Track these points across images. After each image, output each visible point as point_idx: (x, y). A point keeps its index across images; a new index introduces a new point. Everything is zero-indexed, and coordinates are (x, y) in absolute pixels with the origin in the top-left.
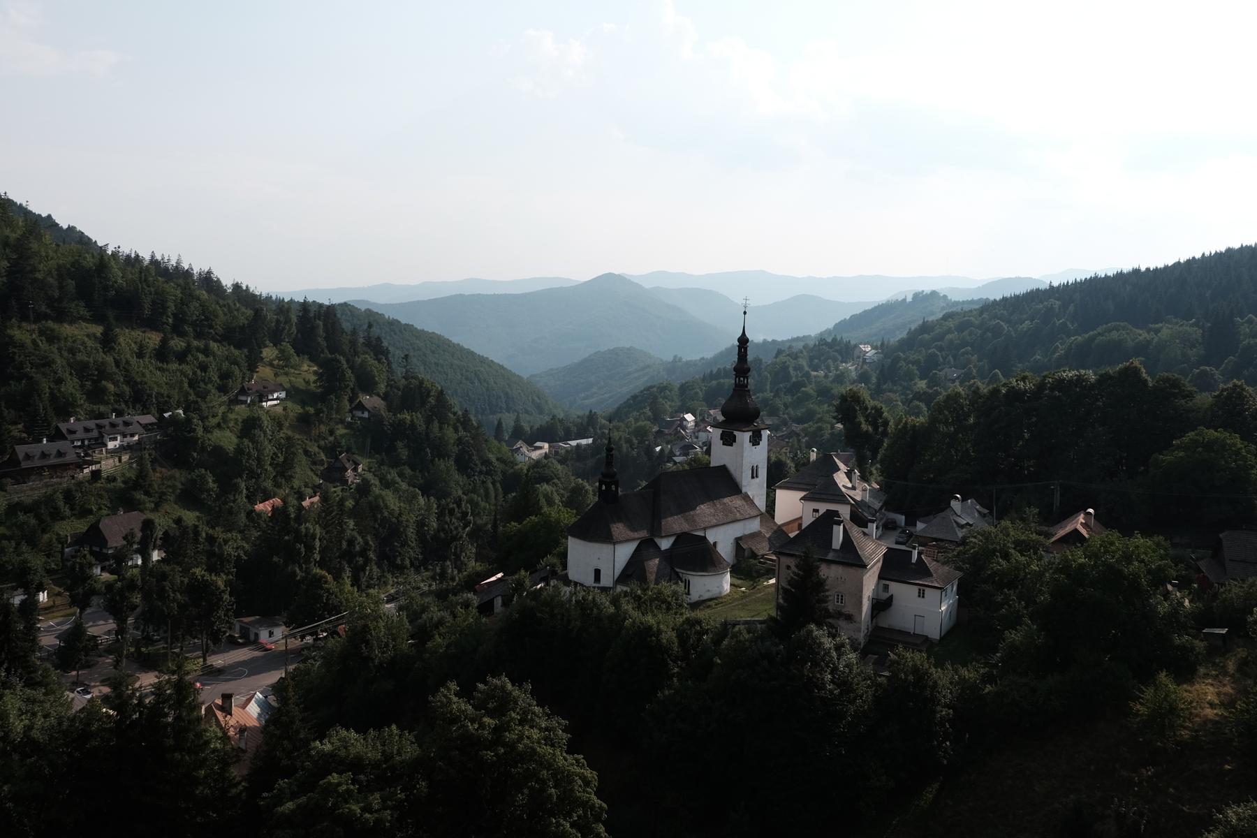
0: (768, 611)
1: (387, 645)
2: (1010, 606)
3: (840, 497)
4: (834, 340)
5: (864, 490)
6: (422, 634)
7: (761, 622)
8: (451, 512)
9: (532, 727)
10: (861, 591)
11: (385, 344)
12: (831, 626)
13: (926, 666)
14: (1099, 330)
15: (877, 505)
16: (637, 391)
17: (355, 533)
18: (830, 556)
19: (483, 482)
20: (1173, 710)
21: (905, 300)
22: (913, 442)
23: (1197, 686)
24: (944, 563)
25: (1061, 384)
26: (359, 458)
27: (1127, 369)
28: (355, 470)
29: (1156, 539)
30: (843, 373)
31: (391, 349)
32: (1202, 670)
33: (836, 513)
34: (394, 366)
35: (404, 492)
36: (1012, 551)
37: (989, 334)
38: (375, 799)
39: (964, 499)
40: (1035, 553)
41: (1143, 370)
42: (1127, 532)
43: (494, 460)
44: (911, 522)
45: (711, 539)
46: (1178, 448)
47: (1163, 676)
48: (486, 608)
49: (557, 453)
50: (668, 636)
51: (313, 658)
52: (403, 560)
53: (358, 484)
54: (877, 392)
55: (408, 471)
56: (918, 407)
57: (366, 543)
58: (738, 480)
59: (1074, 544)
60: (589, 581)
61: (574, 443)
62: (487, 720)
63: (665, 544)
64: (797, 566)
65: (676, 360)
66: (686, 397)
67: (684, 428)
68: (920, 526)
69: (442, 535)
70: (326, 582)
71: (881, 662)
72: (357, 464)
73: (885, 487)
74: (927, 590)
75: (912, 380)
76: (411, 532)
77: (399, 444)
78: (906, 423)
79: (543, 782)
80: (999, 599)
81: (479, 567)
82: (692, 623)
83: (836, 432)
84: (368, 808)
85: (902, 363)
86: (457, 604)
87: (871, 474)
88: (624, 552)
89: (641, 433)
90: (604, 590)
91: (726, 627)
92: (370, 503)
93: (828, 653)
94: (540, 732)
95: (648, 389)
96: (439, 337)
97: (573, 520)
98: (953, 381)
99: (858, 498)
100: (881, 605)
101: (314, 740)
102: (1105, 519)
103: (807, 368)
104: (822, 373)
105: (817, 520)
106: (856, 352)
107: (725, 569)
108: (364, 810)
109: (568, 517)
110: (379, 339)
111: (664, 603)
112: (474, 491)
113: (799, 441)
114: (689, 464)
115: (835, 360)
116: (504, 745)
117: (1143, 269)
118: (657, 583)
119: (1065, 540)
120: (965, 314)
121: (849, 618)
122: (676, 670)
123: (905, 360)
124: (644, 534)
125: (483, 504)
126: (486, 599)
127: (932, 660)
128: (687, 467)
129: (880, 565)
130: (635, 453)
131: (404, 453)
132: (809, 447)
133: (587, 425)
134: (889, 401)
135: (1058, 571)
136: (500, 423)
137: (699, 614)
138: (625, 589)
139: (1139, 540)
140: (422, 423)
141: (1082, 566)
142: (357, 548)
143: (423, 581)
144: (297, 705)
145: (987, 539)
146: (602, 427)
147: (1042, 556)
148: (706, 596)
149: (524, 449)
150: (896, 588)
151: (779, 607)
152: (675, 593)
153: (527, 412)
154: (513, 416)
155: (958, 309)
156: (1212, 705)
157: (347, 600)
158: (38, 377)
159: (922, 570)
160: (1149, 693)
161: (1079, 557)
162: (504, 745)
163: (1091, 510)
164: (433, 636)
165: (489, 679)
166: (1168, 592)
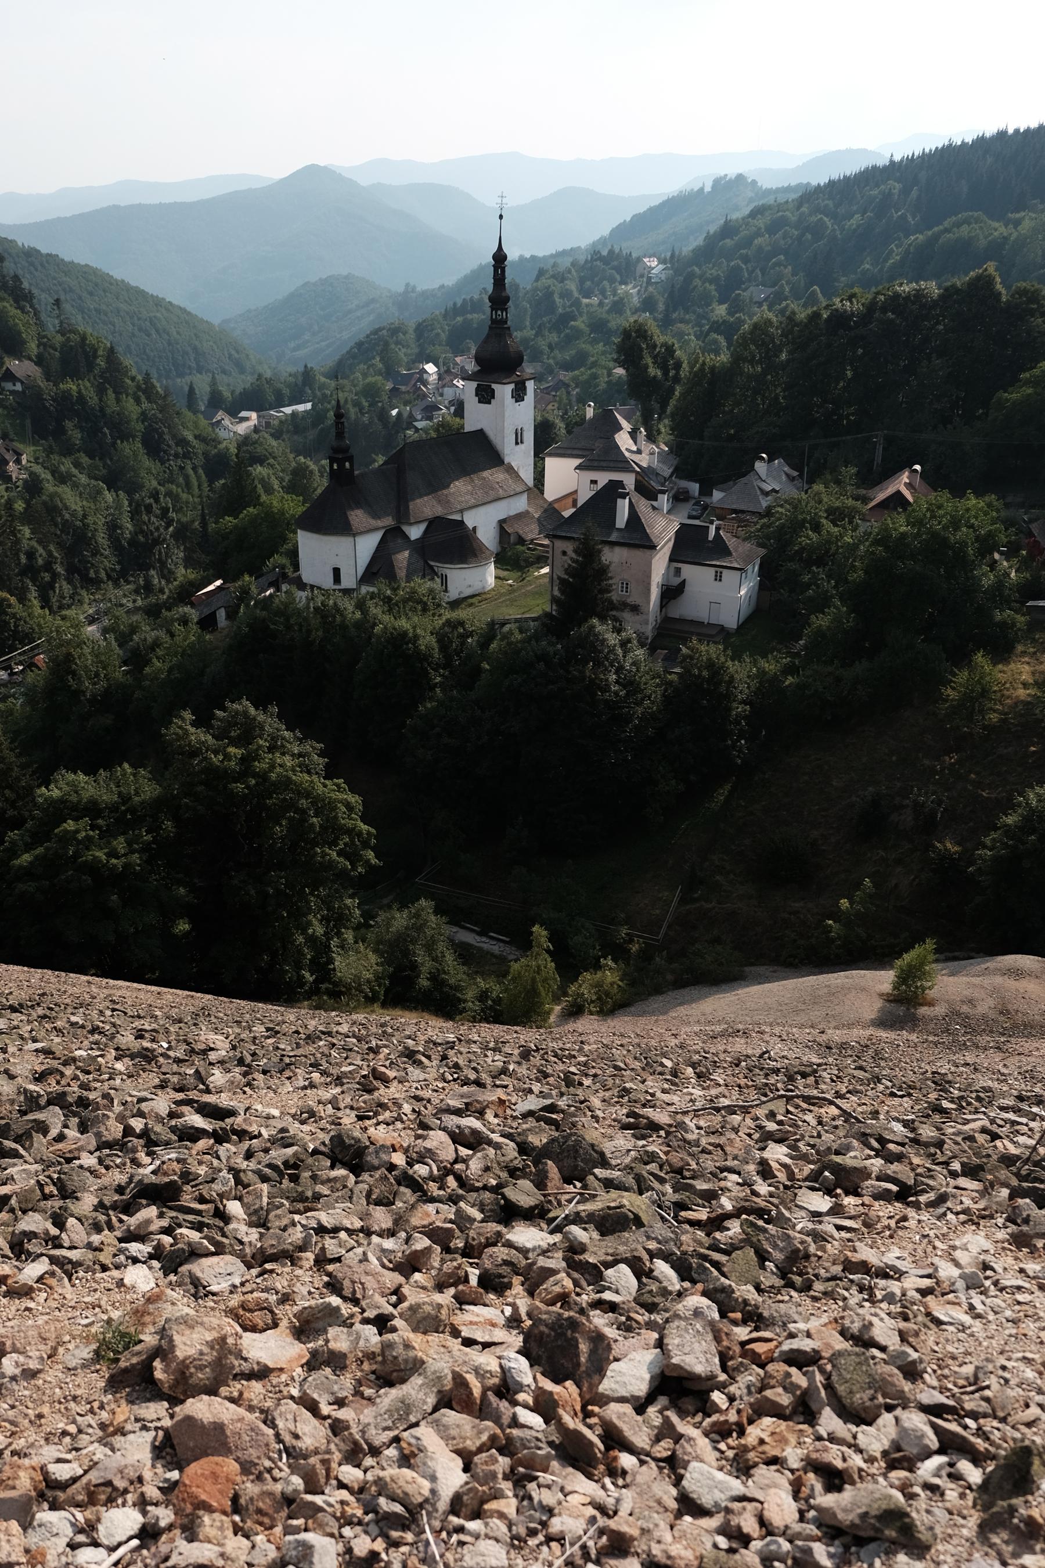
0: (540, 606)
1: (97, 675)
2: (818, 586)
3: (622, 464)
4: (611, 252)
5: (652, 454)
6: (137, 659)
7: (534, 619)
8: (149, 509)
9: (283, 754)
10: (649, 577)
11: (26, 285)
12: (616, 619)
13: (723, 659)
14: (947, 224)
15: (667, 471)
16: (361, 337)
17: (34, 543)
18: (614, 537)
19: (182, 468)
20: (985, 693)
21: (702, 189)
22: (712, 386)
23: (1012, 666)
24: (745, 540)
25: (897, 303)
26: (19, 446)
27: (979, 278)
28: (18, 461)
29: (987, 499)
30: (622, 299)
31: (35, 291)
32: (1020, 648)
33: (620, 484)
34: (43, 316)
35: (85, 487)
36: (824, 521)
37: (809, 236)
38: (120, 844)
39: (771, 460)
40: (850, 522)
41: (998, 280)
42: (958, 492)
43: (190, 438)
44: (705, 491)
45: (470, 523)
46: (1027, 382)
47: (979, 658)
48: (208, 623)
49: (268, 424)
50: (427, 641)
51: (13, 696)
52: (97, 572)
53: (25, 481)
54: (666, 323)
55: (85, 460)
56: (715, 341)
57: (50, 554)
58: (499, 448)
59: (895, 509)
60: (328, 583)
61: (288, 410)
62: (231, 750)
63: (415, 532)
64: (575, 551)
65: (409, 289)
66: (425, 341)
67: (425, 383)
68: (717, 495)
69: (141, 539)
70: (10, 606)
71: (672, 657)
72: (19, 454)
73: (676, 449)
74: (725, 572)
75: (708, 304)
76: (102, 539)
77: (69, 424)
78: (704, 364)
79: (303, 812)
80: (806, 578)
81: (192, 575)
82: (454, 624)
83: (614, 379)
84: (117, 853)
85: (697, 282)
86: (173, 620)
87: (659, 432)
88: (367, 545)
89: (371, 392)
90: (347, 592)
91: (493, 627)
92: (44, 503)
93: (612, 650)
94: (293, 758)
95: (376, 332)
96: (95, 271)
97: (301, 509)
98: (760, 304)
99: (644, 464)
100: (672, 593)
101: (39, 786)
102: (934, 479)
103: (576, 294)
104: (595, 300)
105: (598, 493)
106: (639, 270)
107: (487, 559)
108: (109, 855)
109: (294, 506)
110: (16, 278)
111: (423, 605)
112: (171, 481)
113: (568, 393)
114: (437, 430)
115: (612, 281)
116: (255, 775)
117: (1011, 131)
118: (408, 581)
119: (884, 504)
120: (780, 207)
121: (635, 609)
122: (438, 679)
123: (700, 277)
124: (389, 521)
125: (184, 496)
126: (207, 611)
127: (729, 652)
128: (434, 435)
129: (671, 544)
130: (366, 419)
131: (75, 435)
132: (583, 401)
133: (302, 385)
134: (680, 335)
135: (876, 542)
136: (192, 390)
137: (461, 614)
138: (371, 589)
139: (972, 501)
140: (93, 394)
141: (904, 535)
142: (40, 561)
143: (125, 596)
144: (12, 750)
145: (795, 507)
146: (323, 386)
147: (857, 525)
148: (468, 592)
149: (227, 422)
150: (689, 571)
151: (554, 600)
152: (431, 591)
153: (224, 372)
154: (207, 378)
155: (770, 200)
156: (1025, 685)
157: (39, 625)
158: (706, 1093)
159: (720, 549)
160: (962, 676)
161: (900, 524)
162: (255, 775)
163: (918, 467)
164: (150, 660)
165: (228, 704)
166: (996, 562)
